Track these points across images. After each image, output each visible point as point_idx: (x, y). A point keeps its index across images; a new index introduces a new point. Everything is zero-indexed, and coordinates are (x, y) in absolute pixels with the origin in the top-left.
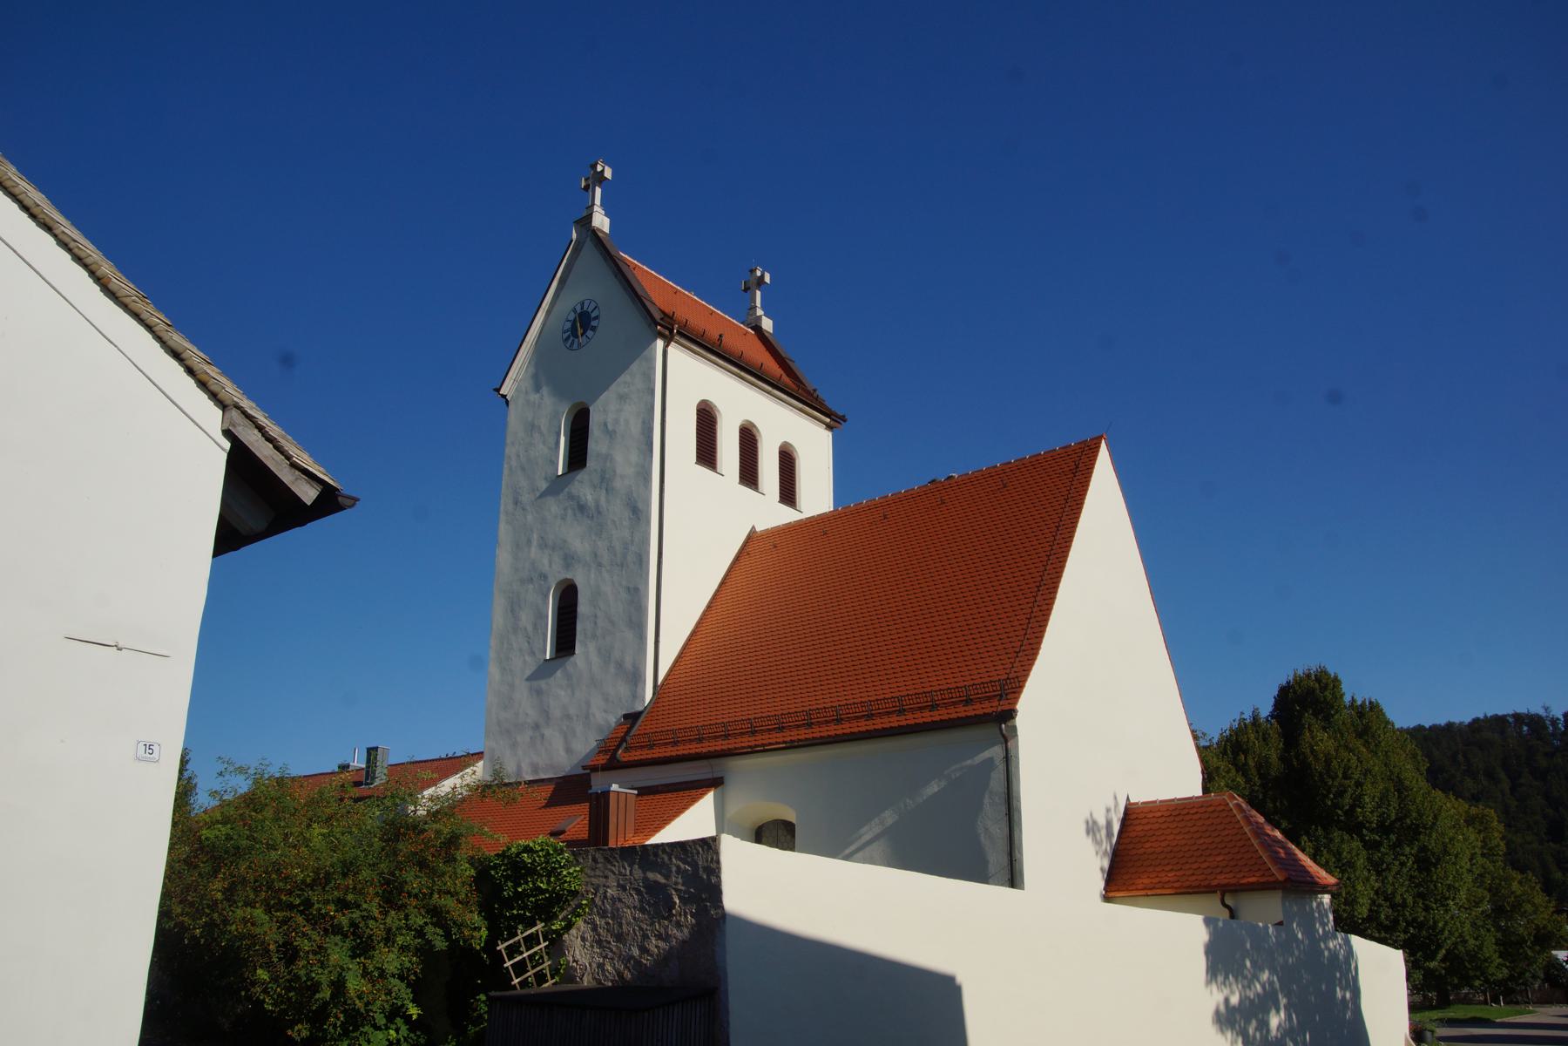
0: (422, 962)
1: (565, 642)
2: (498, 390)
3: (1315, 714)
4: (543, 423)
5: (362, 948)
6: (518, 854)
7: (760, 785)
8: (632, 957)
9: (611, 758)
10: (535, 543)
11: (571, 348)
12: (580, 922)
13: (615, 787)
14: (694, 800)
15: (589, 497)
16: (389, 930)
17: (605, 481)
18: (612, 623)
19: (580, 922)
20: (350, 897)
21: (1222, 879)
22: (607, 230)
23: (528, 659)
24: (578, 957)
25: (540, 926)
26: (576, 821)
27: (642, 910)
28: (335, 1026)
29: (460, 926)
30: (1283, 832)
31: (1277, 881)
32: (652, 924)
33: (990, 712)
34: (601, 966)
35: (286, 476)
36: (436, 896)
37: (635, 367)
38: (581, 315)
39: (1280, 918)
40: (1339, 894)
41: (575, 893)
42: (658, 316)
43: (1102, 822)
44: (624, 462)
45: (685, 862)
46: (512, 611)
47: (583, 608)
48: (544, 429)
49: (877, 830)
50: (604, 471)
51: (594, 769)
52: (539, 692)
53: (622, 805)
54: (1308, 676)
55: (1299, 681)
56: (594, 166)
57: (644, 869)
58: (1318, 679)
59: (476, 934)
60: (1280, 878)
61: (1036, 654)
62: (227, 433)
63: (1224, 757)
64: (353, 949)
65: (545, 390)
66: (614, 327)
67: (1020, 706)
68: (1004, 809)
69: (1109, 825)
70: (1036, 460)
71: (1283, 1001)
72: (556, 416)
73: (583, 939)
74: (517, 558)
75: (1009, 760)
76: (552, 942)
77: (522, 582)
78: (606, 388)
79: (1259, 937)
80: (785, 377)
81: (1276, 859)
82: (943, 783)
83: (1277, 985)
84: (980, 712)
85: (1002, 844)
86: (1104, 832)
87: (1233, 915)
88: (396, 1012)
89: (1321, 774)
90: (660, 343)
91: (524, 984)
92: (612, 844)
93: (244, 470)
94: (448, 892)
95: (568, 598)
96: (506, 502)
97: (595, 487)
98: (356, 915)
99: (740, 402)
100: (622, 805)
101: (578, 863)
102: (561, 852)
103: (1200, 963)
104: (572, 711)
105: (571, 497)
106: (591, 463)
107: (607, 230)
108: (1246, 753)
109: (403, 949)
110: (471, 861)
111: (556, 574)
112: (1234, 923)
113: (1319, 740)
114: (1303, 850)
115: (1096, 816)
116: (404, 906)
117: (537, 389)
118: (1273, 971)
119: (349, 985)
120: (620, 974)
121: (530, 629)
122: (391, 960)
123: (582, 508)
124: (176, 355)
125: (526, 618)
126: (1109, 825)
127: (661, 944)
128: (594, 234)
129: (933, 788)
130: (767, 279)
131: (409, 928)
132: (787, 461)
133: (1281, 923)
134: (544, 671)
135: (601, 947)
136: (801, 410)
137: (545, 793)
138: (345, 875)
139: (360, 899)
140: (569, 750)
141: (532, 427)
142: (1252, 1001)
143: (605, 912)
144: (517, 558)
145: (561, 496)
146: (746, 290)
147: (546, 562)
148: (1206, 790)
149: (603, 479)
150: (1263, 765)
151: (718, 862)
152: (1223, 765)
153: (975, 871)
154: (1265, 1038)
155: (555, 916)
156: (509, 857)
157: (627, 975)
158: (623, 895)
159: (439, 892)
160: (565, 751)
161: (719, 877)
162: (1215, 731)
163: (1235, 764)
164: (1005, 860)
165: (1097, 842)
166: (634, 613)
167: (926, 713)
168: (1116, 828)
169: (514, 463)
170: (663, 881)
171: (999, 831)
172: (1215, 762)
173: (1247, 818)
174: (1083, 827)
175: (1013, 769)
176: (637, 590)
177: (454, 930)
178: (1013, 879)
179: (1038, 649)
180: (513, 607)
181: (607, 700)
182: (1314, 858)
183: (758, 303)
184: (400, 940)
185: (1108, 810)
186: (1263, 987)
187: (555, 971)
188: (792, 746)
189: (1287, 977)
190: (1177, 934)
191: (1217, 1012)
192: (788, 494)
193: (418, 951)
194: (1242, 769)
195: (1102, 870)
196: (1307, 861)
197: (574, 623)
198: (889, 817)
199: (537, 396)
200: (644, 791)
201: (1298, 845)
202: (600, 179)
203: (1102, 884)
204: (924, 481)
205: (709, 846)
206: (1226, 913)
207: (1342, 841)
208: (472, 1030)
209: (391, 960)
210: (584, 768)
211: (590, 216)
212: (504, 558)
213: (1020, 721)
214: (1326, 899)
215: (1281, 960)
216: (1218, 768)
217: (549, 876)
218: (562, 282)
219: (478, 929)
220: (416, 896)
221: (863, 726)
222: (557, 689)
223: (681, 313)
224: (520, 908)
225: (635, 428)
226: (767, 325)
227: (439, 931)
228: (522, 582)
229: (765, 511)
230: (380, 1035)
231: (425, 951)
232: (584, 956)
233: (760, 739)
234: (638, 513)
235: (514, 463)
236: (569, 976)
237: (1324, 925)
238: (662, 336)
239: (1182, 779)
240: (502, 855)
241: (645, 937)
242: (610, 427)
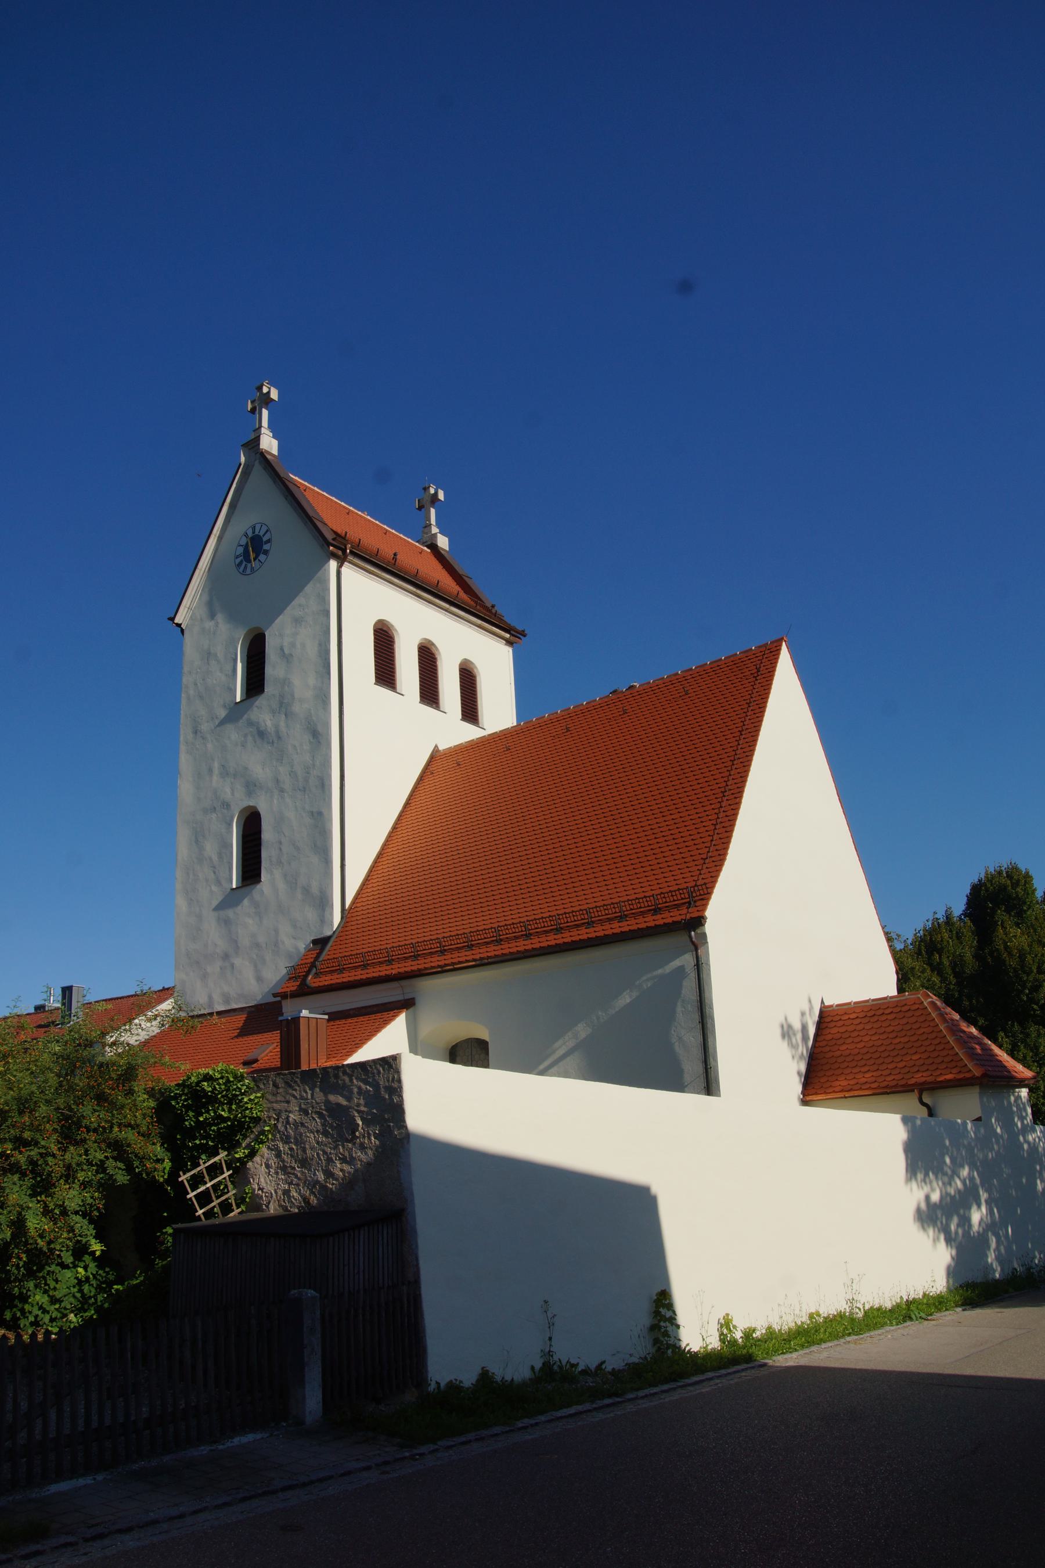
0: (105, 1197)
1: (251, 872)
2: (172, 619)
3: (1008, 911)
4: (220, 651)
5: (42, 1187)
6: (198, 1083)
7: (452, 1003)
8: (318, 1182)
9: (301, 984)
10: (216, 771)
11: (244, 573)
12: (264, 1149)
13: (305, 1013)
14: (386, 1022)
15: (269, 723)
16: (68, 1167)
17: (284, 707)
18: (298, 849)
19: (264, 1149)
20: (27, 1135)
21: (919, 1078)
23: (214, 888)
24: (263, 1184)
25: (223, 1155)
26: (267, 1049)
27: (325, 1133)
28: (18, 1267)
29: (142, 1159)
30: (980, 1029)
31: (974, 1078)
32: (336, 1147)
33: (678, 919)
34: (286, 1192)
36: (116, 1129)
37: (308, 588)
38: (253, 539)
39: (978, 1114)
40: (1038, 1088)
41: (257, 1120)
42: (330, 537)
43: (797, 1026)
44: (302, 685)
45: (366, 1083)
46: (197, 841)
47: (267, 834)
48: (220, 655)
49: (571, 1044)
50: (282, 696)
51: (284, 996)
52: (227, 922)
54: (1000, 873)
55: (990, 878)
56: (260, 388)
57: (325, 1091)
58: (1009, 876)
59: (159, 1166)
63: (920, 957)
64: (33, 1188)
65: (220, 617)
66: (283, 550)
67: (709, 913)
68: (697, 1017)
69: (804, 1028)
70: (717, 664)
71: (984, 1196)
72: (232, 642)
73: (268, 1166)
74: (200, 791)
75: (700, 968)
76: (236, 1171)
77: (205, 811)
78: (280, 611)
79: (957, 1133)
80: (463, 595)
81: (972, 1055)
82: (635, 994)
83: (978, 1181)
84: (669, 920)
85: (697, 1052)
86: (799, 1036)
87: (931, 1114)
88: (80, 1251)
89: (1015, 970)
91: (209, 1214)
92: (304, 1067)
94: (129, 1125)
96: (185, 732)
97: (273, 712)
98: (34, 1153)
99: (417, 620)
101: (259, 1089)
102: (241, 1078)
103: (899, 1161)
104: (262, 939)
105: (250, 724)
106: (269, 688)
108: (940, 952)
109: (84, 1185)
110: (151, 1093)
111: (240, 801)
112: (932, 1121)
113: (1013, 936)
114: (1000, 1047)
115: (791, 1020)
116: (84, 1141)
117: (212, 616)
118: (973, 1166)
119: (29, 1224)
120: (306, 1200)
121: (215, 858)
122: (72, 1197)
123: (261, 734)
125: (210, 848)
126: (804, 1028)
127: (346, 1167)
128: (263, 456)
129: (625, 999)
130: (441, 496)
131: (90, 1163)
132: (468, 678)
133: (979, 1119)
134: (231, 899)
135: (286, 1173)
136: (479, 626)
137: (240, 1019)
138: (21, 1113)
139: (38, 1136)
140: (259, 979)
141: (208, 656)
142: (953, 1198)
143: (288, 1137)
144: (200, 791)
145: (242, 722)
146: (420, 508)
147: (228, 790)
148: (900, 990)
149: (281, 704)
150: (957, 964)
151: (399, 1081)
152: (917, 965)
153: (673, 1082)
154: (967, 1233)
155: (238, 1144)
156: (190, 1086)
157: (313, 1201)
158: (305, 1120)
159: (120, 1125)
160: (255, 980)
161: (401, 1096)
162: (910, 930)
163: (930, 964)
164: (700, 1068)
165: (793, 1046)
166: (319, 838)
168: (812, 1031)
169: (192, 692)
170: (344, 1103)
171: (693, 1039)
172: (909, 962)
173: (942, 1016)
174: (778, 1032)
175: (704, 976)
176: (320, 814)
177: (136, 1163)
178: (709, 1086)
179: (725, 854)
180: (198, 837)
181: (295, 926)
182: (1011, 1054)
184: (81, 1176)
185: (803, 1014)
186: (964, 1182)
187: (240, 1200)
188: (482, 963)
189: (987, 1171)
190: (874, 1135)
191: (918, 1210)
192: (470, 712)
193: (102, 1186)
194: (937, 969)
195: (799, 1073)
196: (1003, 1056)
198: (582, 1030)
199: (212, 623)
200: (334, 1017)
201: (995, 1041)
202: (266, 400)
203: (799, 1088)
204: (606, 691)
205: (390, 1064)
206: (925, 1110)
207: (1039, 1035)
208: (159, 1263)
209: (72, 1197)
210: (275, 995)
211: (257, 440)
212: (186, 788)
213: (709, 928)
214: (1024, 1092)
215: (981, 1156)
216: (913, 969)
217: (230, 1103)
218: (233, 506)
220: (95, 1130)
222: (246, 918)
223: (354, 533)
224: (202, 1138)
225: (312, 650)
226: (443, 542)
227: (120, 1165)
228: (205, 811)
229: (449, 729)
230: (68, 1274)
231: (108, 1187)
232: (269, 1183)
234: (318, 736)
235: (192, 692)
236: (255, 1205)
237: (1022, 1118)
238: (334, 556)
239: (875, 979)
240: (182, 1085)
241: (329, 1160)
242: (287, 651)
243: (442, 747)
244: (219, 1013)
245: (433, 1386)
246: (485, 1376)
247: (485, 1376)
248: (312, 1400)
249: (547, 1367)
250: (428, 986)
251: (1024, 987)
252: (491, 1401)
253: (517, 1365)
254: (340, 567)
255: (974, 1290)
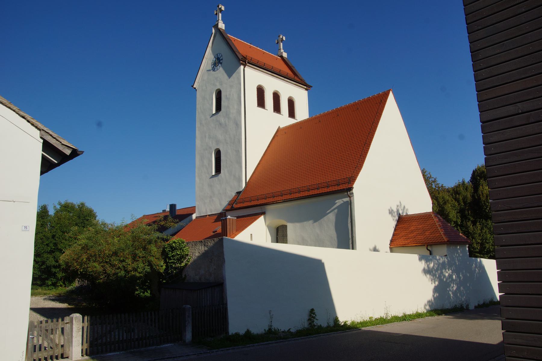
1: (218, 170)
2: (193, 86)
3: (485, 180)
9: (231, 208)
14: (255, 220)
15: (223, 121)
22: (224, 28)
31: (445, 242)
35: (61, 148)
41: (187, 255)
42: (240, 57)
47: (223, 158)
53: (231, 222)
60: (446, 241)
61: (361, 168)
62: (41, 138)
70: (369, 99)
84: (342, 188)
87: (431, 254)
89: (484, 201)
90: (242, 67)
93: (47, 146)
95: (218, 154)
98: (124, 264)
99: (272, 84)
100: (231, 222)
107: (224, 28)
108: (459, 194)
123: (221, 124)
124: (23, 117)
130: (284, 39)
132: (291, 103)
140: (221, 204)
150: (464, 199)
155: (183, 262)
167: (336, 187)
176: (238, 151)
183: (282, 48)
188: (285, 201)
192: (292, 114)
194: (457, 200)
197: (220, 163)
200: (238, 217)
211: (218, 24)
212: (198, 142)
213: (354, 191)
216: (448, 200)
219: (162, 266)
221: (307, 194)
226: (285, 55)
229: (284, 120)
233: (276, 199)
234: (238, 125)
243: (281, 127)
244: (209, 215)
245: (230, 334)
246: (248, 332)
247: (248, 332)
248: (188, 336)
249: (270, 329)
250: (269, 208)
251: (487, 207)
252: (248, 338)
253: (258, 327)
254: (244, 67)
255: (437, 310)
